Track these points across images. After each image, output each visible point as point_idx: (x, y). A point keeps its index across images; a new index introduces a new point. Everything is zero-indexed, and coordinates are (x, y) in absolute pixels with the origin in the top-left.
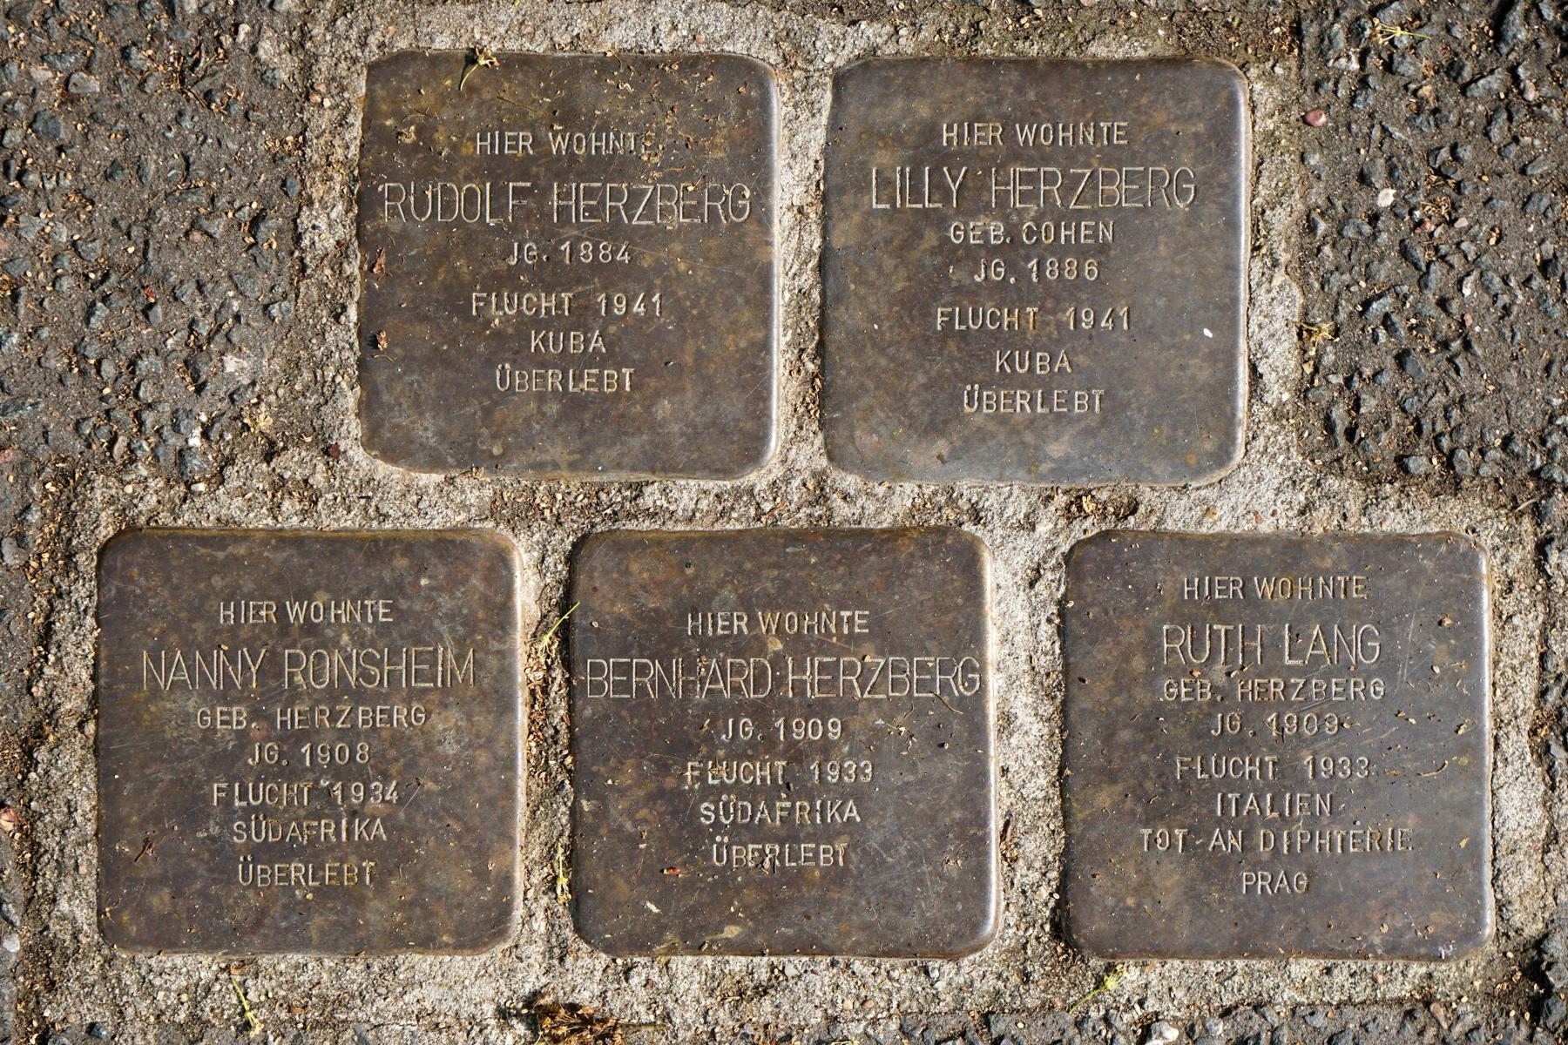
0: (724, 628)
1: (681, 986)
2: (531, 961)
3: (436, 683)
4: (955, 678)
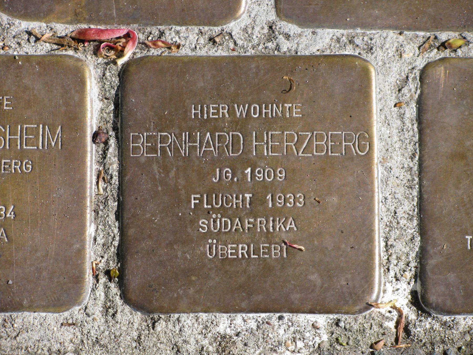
0: (213, 114)
1: (187, 331)
2: (95, 316)
3: (158, 155)
4: (354, 145)
